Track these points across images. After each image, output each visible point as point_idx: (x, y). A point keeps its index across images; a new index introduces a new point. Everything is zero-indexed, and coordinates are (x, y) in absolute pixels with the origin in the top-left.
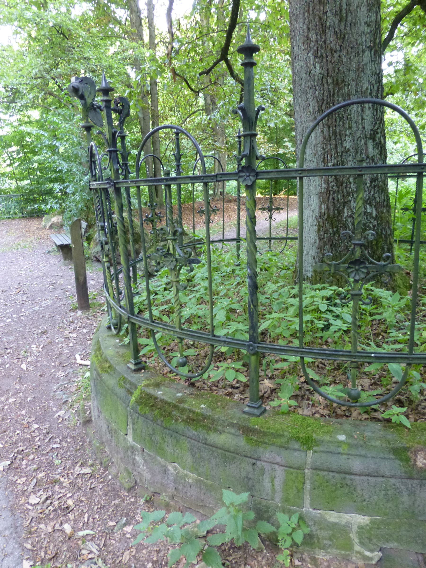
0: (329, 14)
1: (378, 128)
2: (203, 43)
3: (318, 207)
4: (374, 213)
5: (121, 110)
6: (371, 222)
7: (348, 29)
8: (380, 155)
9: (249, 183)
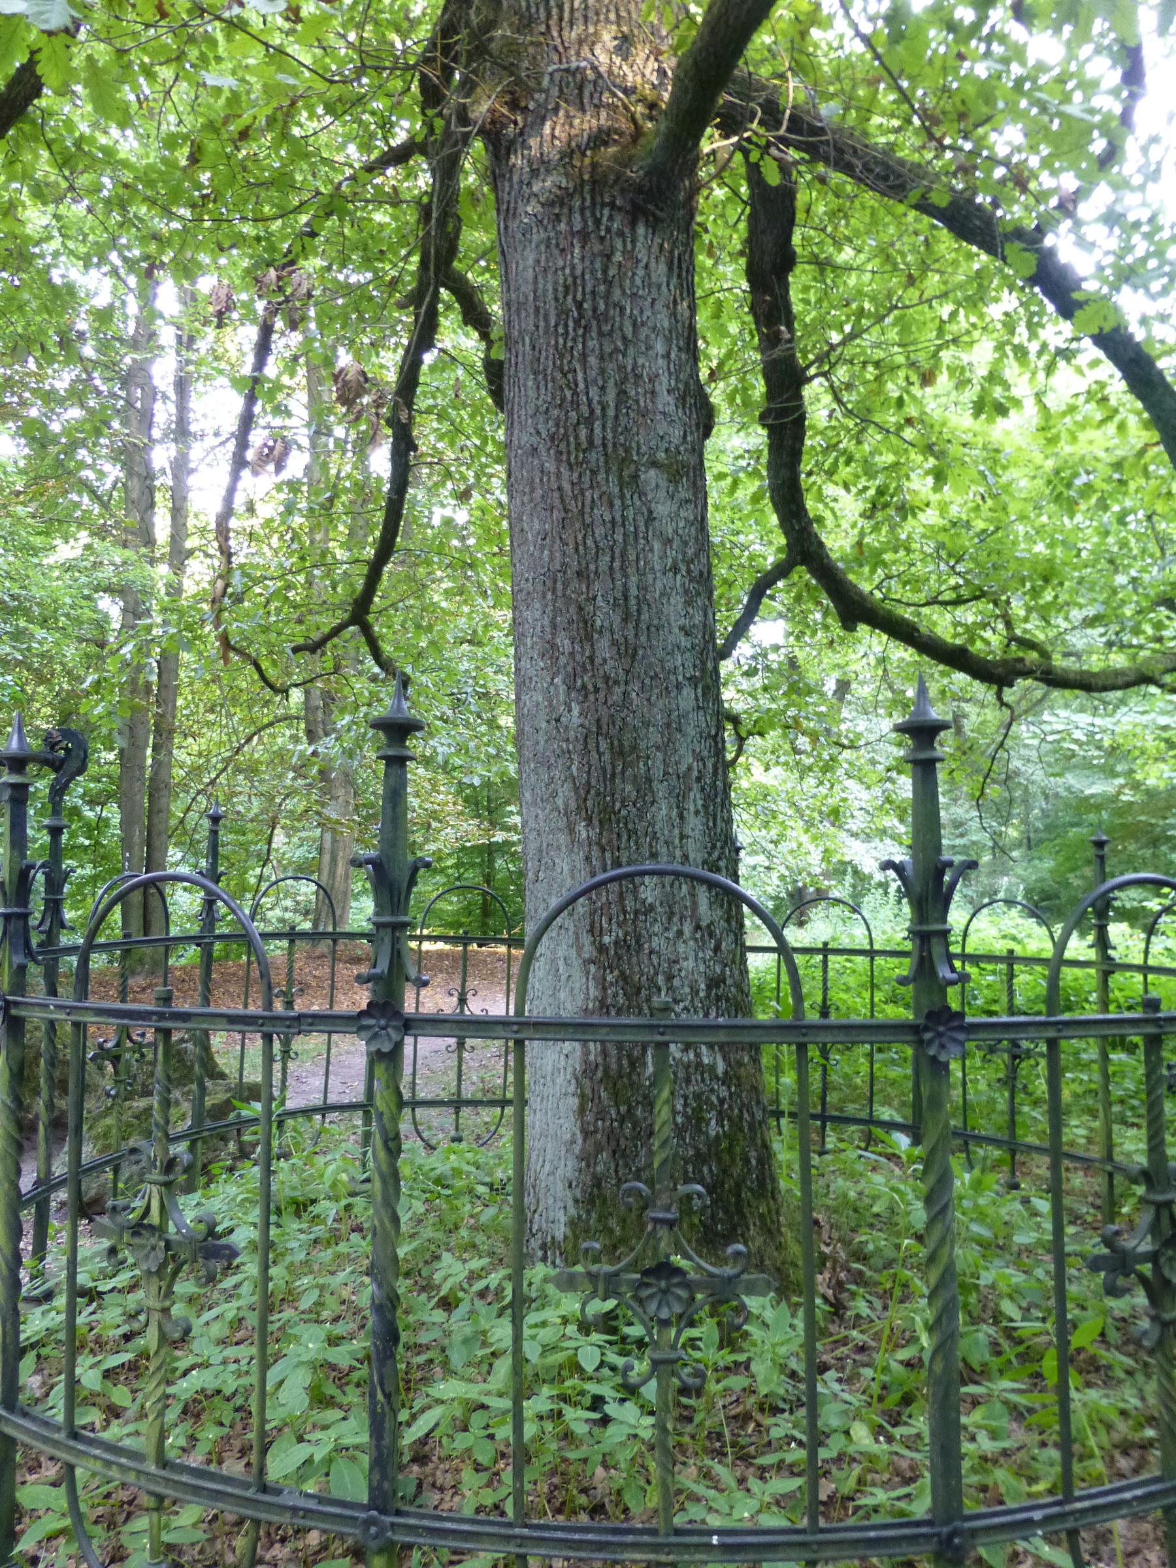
0: (600, 602)
2: (309, 583)
4: (721, 1067)
5: (63, 761)
7: (643, 638)
8: (728, 921)
9: (387, 1048)
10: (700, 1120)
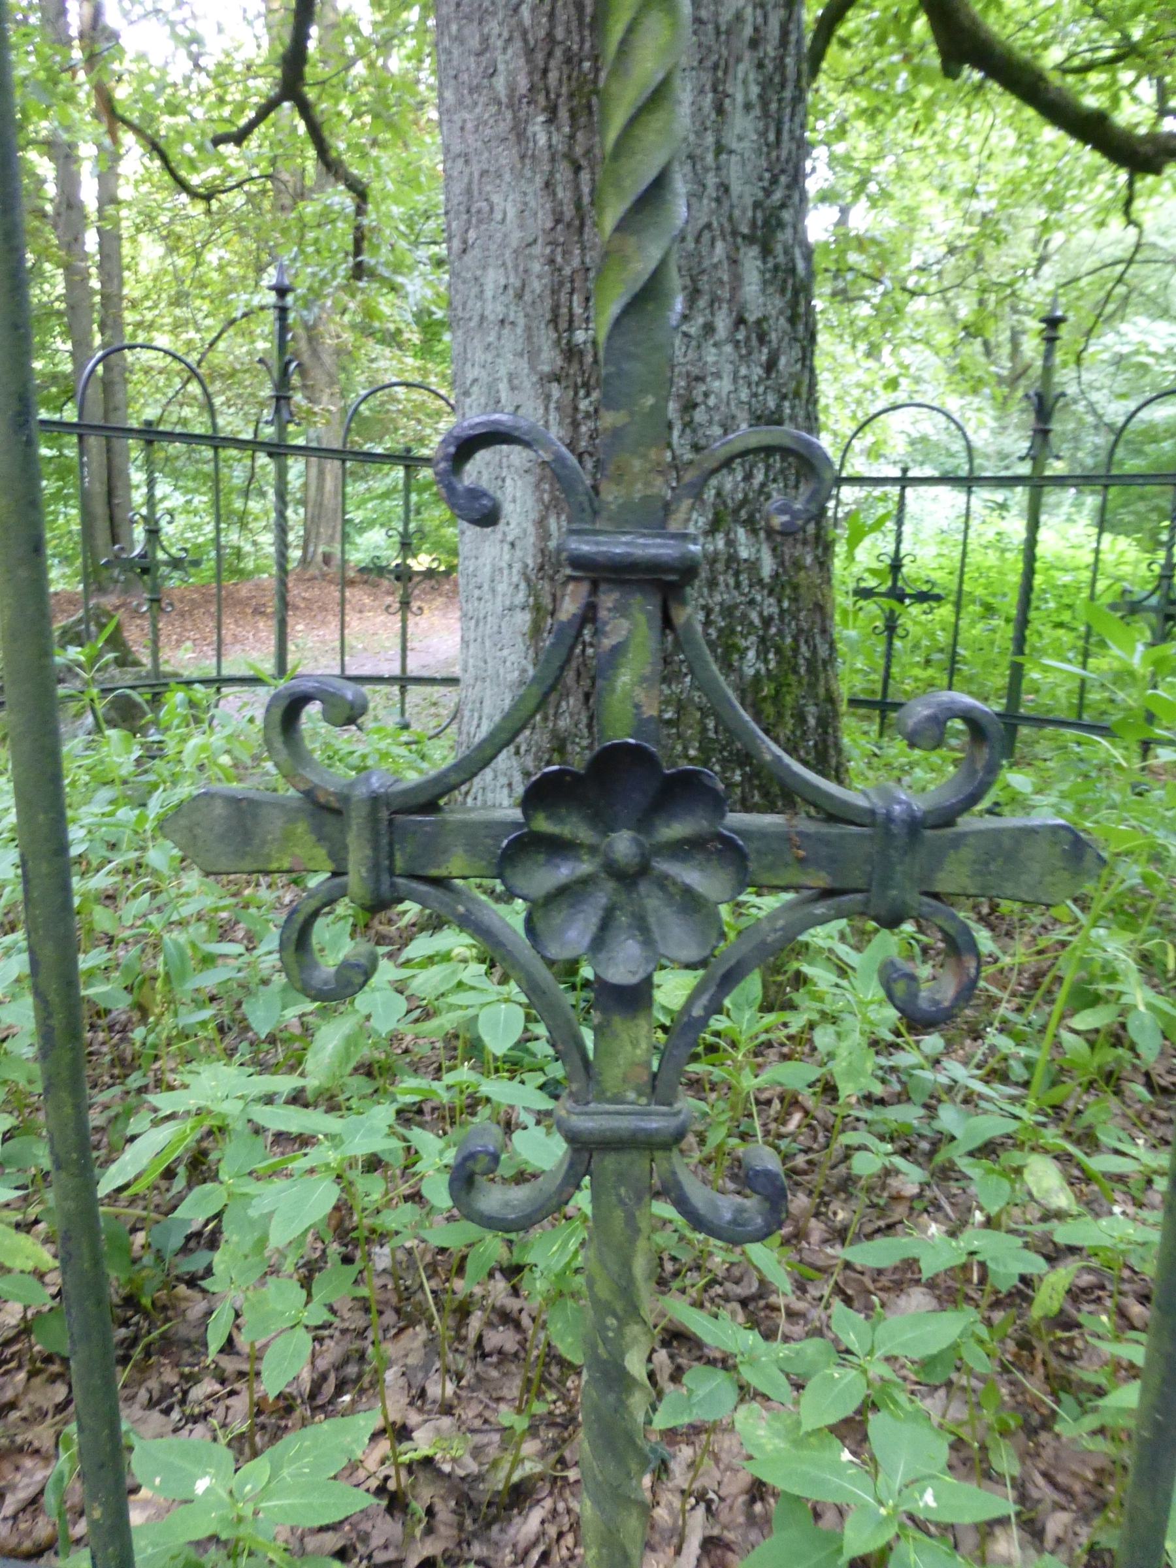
1: (783, 206)
3: (531, 529)
4: (768, 566)
6: (752, 602)
8: (792, 320)
10: (731, 648)
